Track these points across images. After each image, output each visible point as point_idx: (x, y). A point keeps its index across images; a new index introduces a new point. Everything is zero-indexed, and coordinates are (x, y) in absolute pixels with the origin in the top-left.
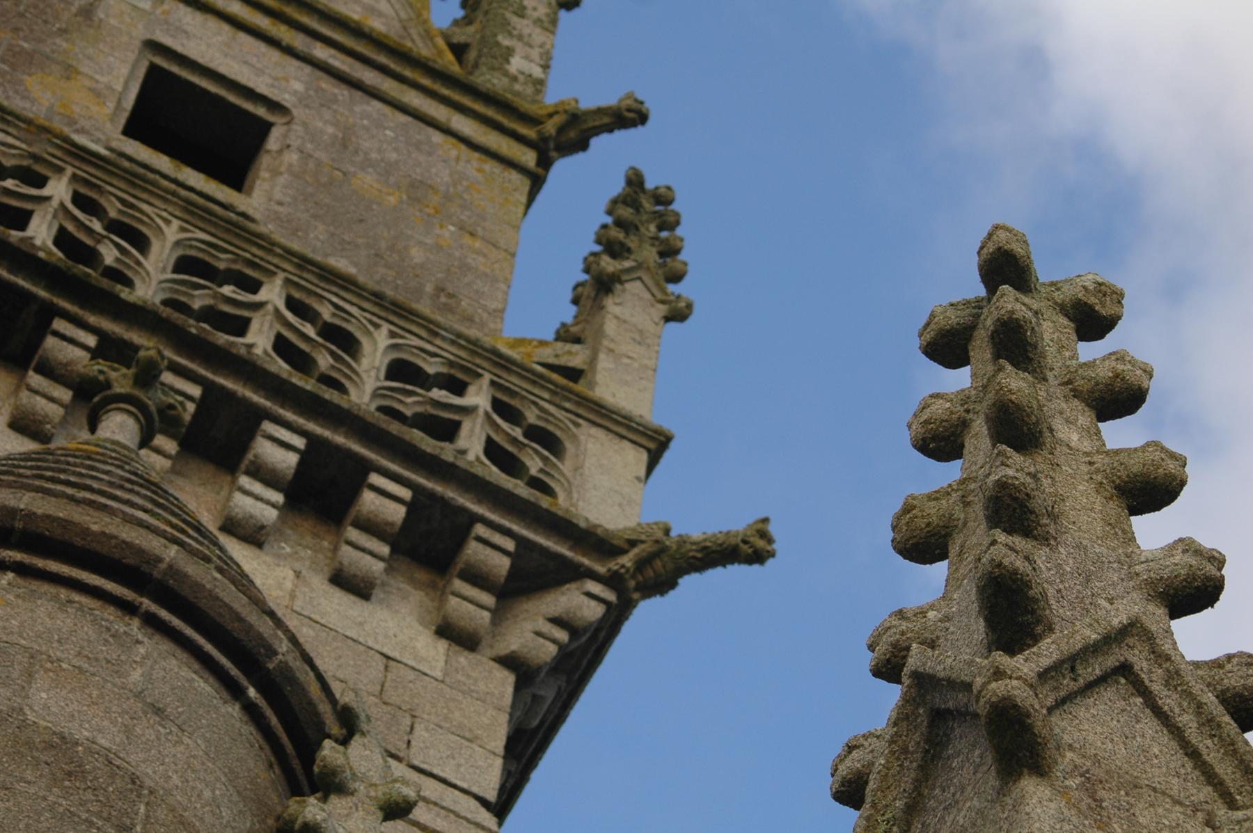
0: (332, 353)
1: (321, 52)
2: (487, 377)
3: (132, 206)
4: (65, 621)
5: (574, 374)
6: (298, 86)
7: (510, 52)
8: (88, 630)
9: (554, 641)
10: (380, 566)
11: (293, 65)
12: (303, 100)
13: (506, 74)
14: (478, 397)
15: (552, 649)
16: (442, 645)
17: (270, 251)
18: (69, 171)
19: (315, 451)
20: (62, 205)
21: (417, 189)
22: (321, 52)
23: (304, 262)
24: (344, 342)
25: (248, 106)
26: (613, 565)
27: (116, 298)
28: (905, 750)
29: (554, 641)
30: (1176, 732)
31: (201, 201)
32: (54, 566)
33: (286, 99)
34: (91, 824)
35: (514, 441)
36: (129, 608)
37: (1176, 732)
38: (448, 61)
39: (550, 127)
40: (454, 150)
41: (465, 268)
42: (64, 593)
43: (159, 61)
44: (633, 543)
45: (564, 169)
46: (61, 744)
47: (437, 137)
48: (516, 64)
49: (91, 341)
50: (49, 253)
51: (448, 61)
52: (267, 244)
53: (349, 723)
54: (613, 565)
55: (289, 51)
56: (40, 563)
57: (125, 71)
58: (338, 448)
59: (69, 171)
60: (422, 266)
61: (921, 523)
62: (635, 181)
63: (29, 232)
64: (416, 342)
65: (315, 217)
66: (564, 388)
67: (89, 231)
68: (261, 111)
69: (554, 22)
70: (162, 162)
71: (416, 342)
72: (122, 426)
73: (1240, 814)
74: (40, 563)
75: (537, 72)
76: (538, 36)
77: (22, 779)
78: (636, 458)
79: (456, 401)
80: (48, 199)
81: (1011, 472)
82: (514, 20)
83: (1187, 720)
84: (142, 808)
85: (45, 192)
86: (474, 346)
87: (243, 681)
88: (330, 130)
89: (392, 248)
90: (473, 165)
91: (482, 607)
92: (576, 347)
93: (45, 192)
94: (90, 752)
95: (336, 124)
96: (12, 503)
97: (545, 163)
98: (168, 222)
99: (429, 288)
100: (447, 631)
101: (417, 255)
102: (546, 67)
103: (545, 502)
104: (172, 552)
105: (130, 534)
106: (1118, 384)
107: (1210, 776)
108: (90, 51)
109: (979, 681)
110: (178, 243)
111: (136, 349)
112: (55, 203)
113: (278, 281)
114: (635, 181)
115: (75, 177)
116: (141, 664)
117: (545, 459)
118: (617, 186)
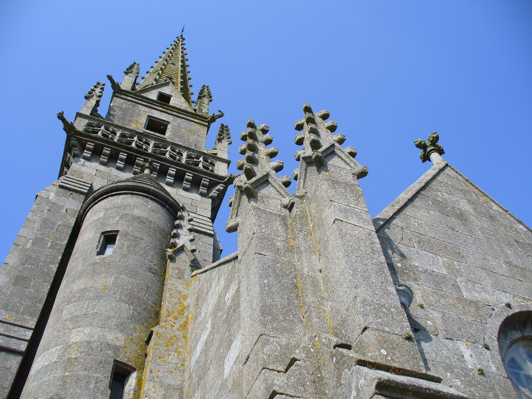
0: (179, 156)
1: (174, 113)
2: (202, 156)
3: (147, 139)
4: (138, 200)
5: (216, 154)
6: (171, 119)
7: (202, 109)
8: (142, 201)
9: (217, 193)
10: (189, 186)
11: (170, 116)
12: (172, 121)
13: (202, 112)
14: (201, 159)
15: (217, 194)
16: (200, 196)
17: (168, 143)
18: (137, 136)
19: (178, 171)
20: (136, 141)
21: (190, 131)
22: (174, 113)
23: (173, 144)
24: (180, 154)
25: (164, 123)
26: (224, 181)
27: (145, 153)
28: (237, 197)
29: (217, 193)
30: (275, 188)
31: (157, 137)
32: (136, 192)
33: (170, 121)
34: (145, 229)
35: (207, 165)
36: (147, 197)
37: (275, 188)
38: (193, 112)
39: (209, 119)
40: (196, 124)
41: (199, 141)
42: (138, 196)
43: (150, 118)
44: (226, 177)
45: (212, 125)
46: (139, 218)
47: (193, 123)
48: (204, 111)
49: (143, 160)
50: (135, 148)
51: (193, 112)
52: (168, 142)
53: (183, 209)
54: (224, 181)
55: (169, 114)
56: (134, 192)
57: (145, 120)
58: (181, 170)
59: (137, 136)
60: (192, 142)
61: (240, 164)
62: (222, 125)
63: (132, 145)
64: (191, 153)
65: (176, 137)
66: (214, 156)
67: (141, 144)
68: (166, 123)
69: (209, 104)
70: (152, 133)
71: (191, 153)
72: (148, 171)
73: (285, 199)
74: (134, 192)
75: (207, 111)
76: (207, 106)
77: (134, 224)
78: (226, 165)
79: (198, 160)
80: (134, 140)
81: (249, 154)
82: (203, 104)
83: (277, 186)
84: (152, 225)
85: (134, 139)
86: (200, 152)
87: (166, 205)
88: (177, 124)
89: (187, 140)
90: (198, 126)
91: (206, 190)
92: (216, 150)
93: (134, 139)
94: (143, 218)
95: (177, 123)
96: (129, 184)
97: (209, 124)
98: (152, 141)
99: (194, 145)
100: (202, 195)
101: (191, 140)
102: (208, 110)
103: (213, 173)
104: (152, 188)
105: (146, 186)
106: (268, 140)
107: (280, 194)
108: (140, 118)
109: (243, 185)
110: (154, 144)
111: (149, 159)
112: (135, 141)
113: (170, 147)
114: (222, 125)
115: (138, 137)
116: (150, 205)
117: (212, 167)
118: (220, 126)
